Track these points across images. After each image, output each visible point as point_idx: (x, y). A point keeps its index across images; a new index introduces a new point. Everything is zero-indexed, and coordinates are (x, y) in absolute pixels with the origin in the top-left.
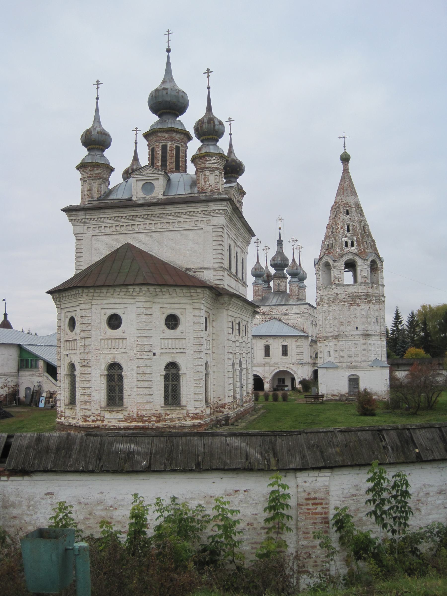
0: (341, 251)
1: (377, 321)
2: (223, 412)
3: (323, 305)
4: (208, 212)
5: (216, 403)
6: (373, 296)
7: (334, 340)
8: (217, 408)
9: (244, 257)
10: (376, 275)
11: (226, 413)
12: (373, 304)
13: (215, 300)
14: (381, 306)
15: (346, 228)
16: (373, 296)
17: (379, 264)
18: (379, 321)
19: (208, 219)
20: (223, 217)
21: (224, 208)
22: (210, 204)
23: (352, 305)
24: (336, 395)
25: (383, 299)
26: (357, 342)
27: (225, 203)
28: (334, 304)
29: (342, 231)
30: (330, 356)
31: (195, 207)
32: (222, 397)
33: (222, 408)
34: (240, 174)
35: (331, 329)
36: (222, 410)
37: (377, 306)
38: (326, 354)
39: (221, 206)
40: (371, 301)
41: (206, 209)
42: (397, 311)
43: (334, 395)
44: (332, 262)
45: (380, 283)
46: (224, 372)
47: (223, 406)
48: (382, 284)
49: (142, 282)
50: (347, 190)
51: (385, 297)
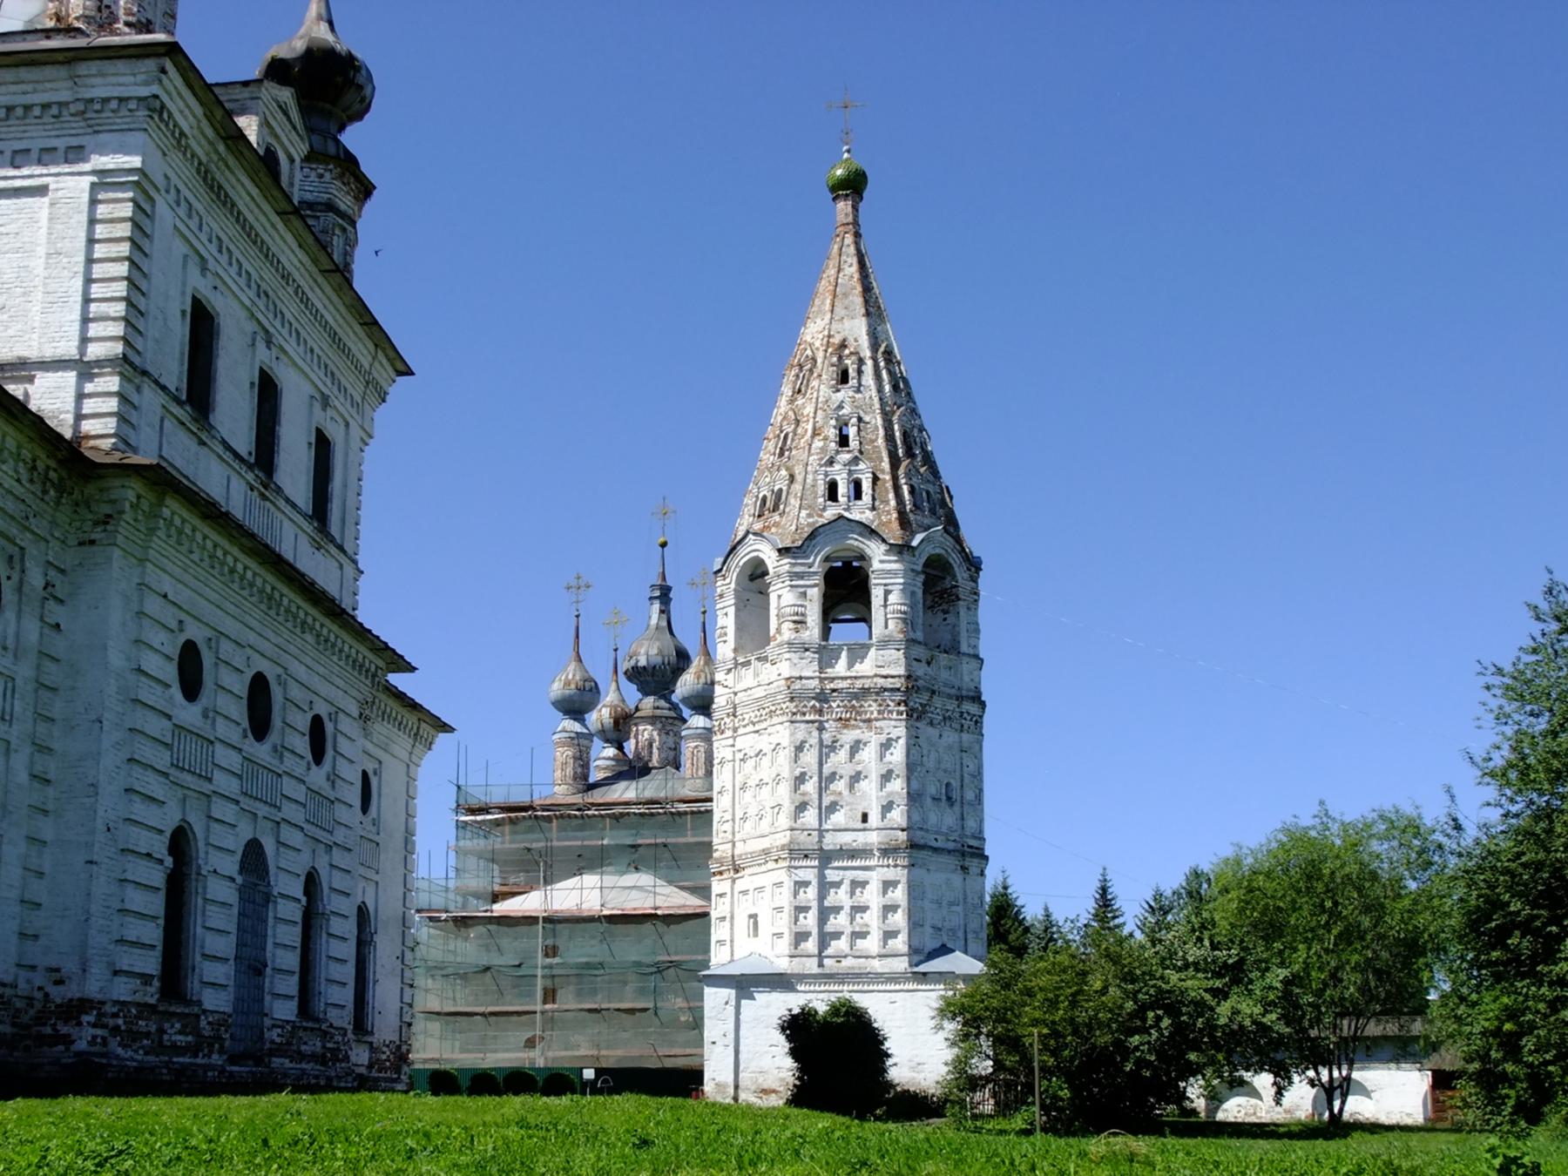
0: (809, 516)
1: (949, 798)
2: (68, 1040)
3: (735, 730)
4: (73, 108)
5: (39, 995)
6: (933, 692)
7: (771, 865)
8: (40, 1019)
9: (335, 433)
10: (951, 619)
11: (82, 1045)
12: (931, 723)
13: (61, 489)
14: (965, 736)
15: (832, 433)
16: (933, 692)
17: (961, 574)
18: (955, 795)
19: (74, 142)
20: (142, 135)
21: (144, 92)
22: (83, 68)
23: (846, 727)
24: (774, 1091)
25: (973, 708)
26: (861, 875)
27: (150, 65)
28: (775, 720)
29: (821, 444)
30: (756, 935)
31: (13, 88)
32: (70, 966)
33: (66, 1022)
34: (359, 116)
35: (765, 826)
36: (64, 1030)
37: (950, 737)
38: (742, 923)
39: (130, 81)
40: (924, 712)
41: (65, 96)
42: (1104, 890)
43: (765, 1091)
44: (775, 555)
45: (964, 648)
46: (89, 846)
47: (76, 1008)
48: (971, 651)
49: (559, 927)
50: (845, 295)
51: (983, 705)
